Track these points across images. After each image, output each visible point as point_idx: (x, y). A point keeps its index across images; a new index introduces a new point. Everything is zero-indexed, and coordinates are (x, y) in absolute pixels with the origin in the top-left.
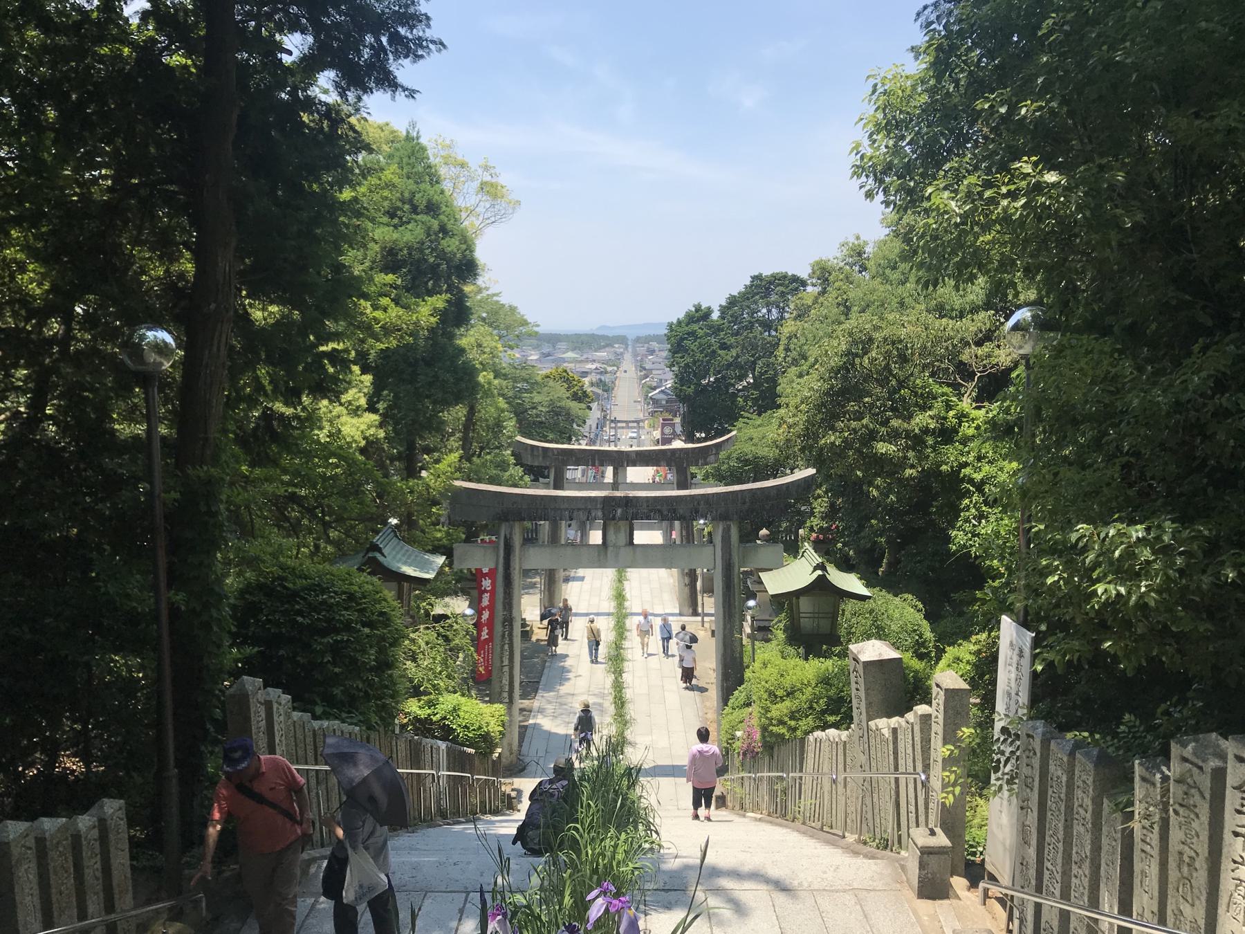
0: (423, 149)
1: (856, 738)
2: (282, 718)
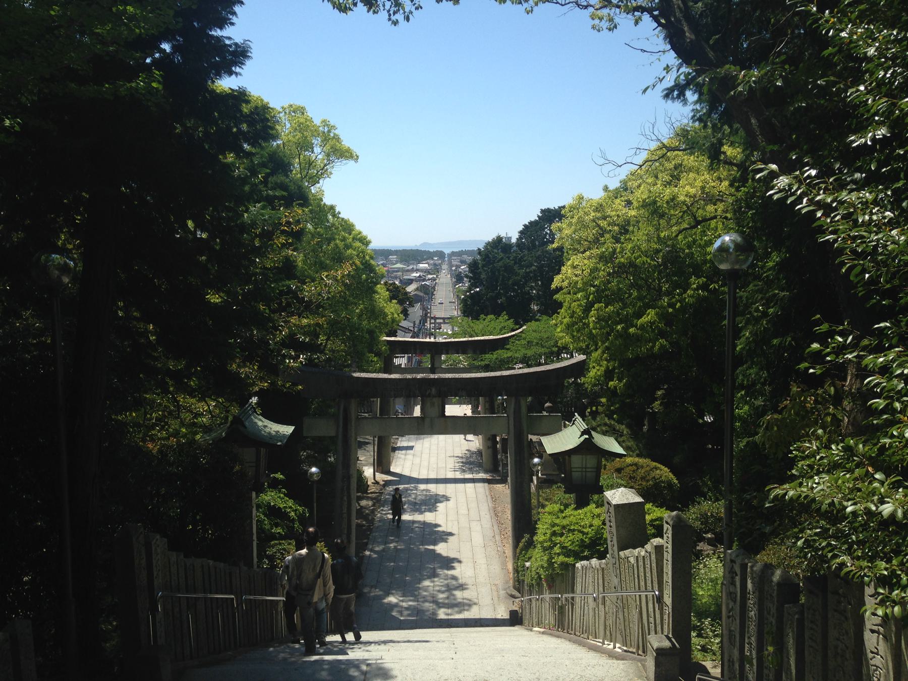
1: (610, 566)
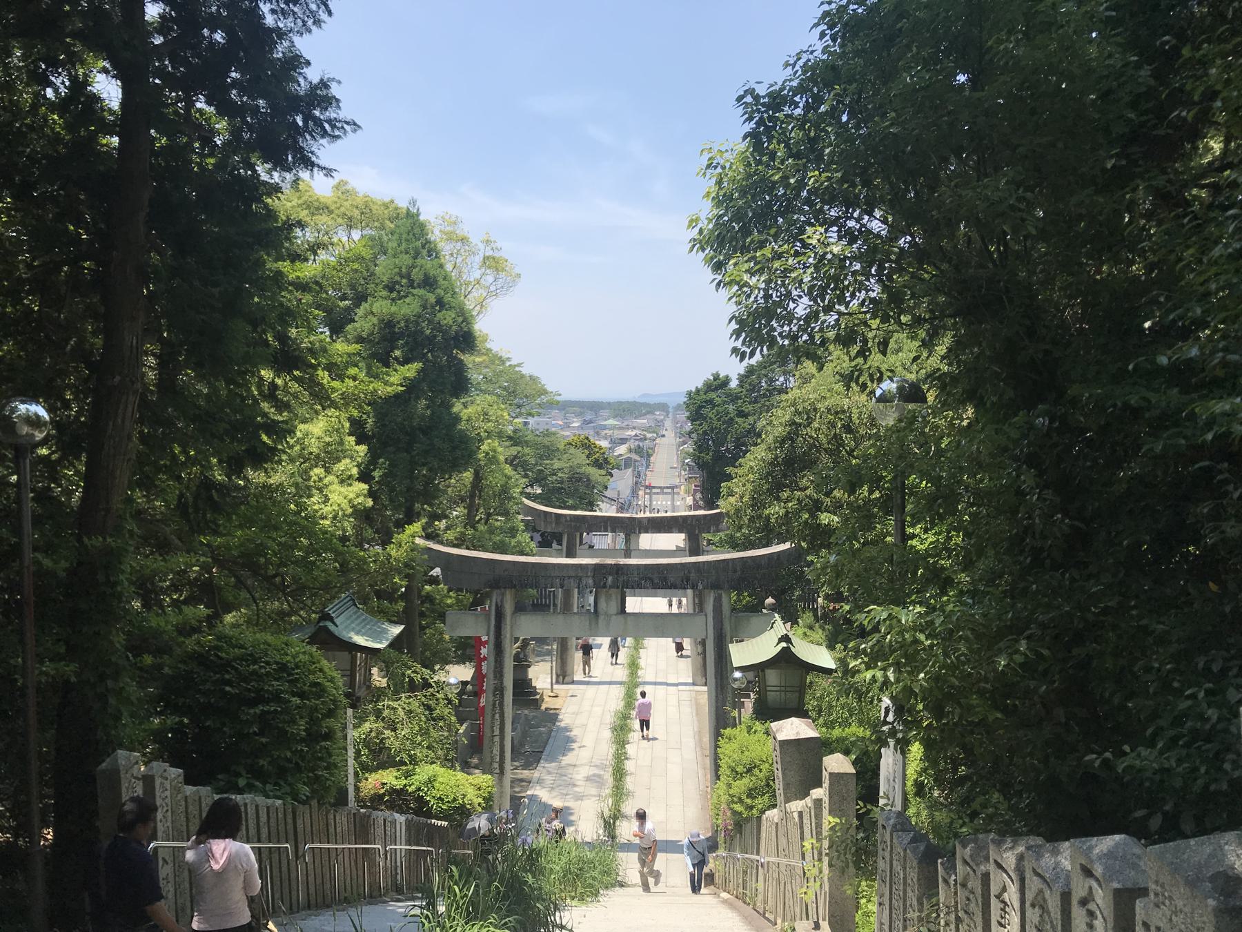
0: (422, 226)
2: (168, 793)
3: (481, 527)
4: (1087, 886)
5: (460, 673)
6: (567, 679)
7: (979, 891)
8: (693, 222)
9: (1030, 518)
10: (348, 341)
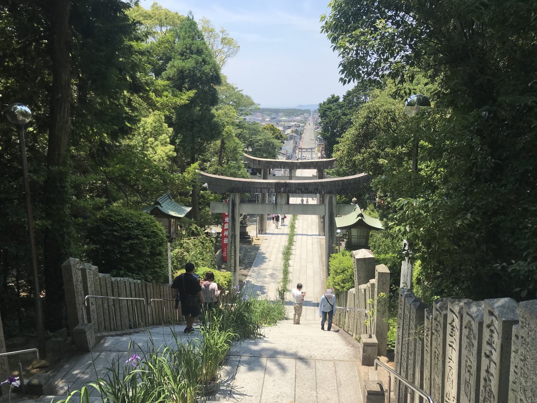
0: (196, 23)
3: (225, 166)
4: (490, 319)
5: (215, 230)
6: (263, 232)
7: (442, 322)
8: (323, 18)
9: (475, 159)
10: (163, 79)
